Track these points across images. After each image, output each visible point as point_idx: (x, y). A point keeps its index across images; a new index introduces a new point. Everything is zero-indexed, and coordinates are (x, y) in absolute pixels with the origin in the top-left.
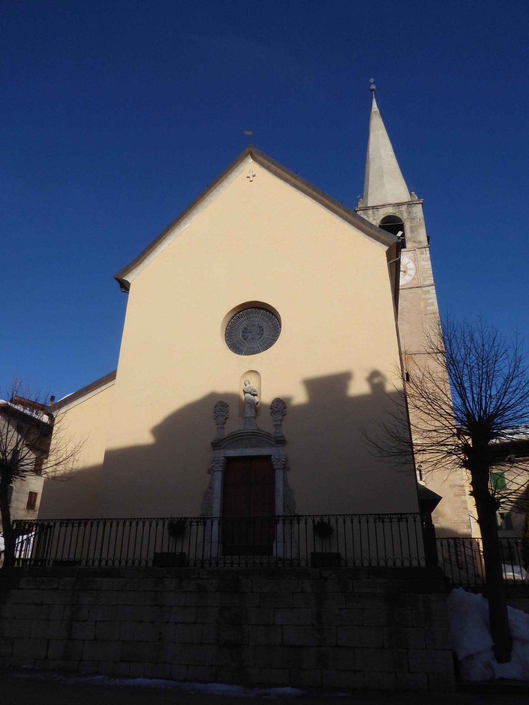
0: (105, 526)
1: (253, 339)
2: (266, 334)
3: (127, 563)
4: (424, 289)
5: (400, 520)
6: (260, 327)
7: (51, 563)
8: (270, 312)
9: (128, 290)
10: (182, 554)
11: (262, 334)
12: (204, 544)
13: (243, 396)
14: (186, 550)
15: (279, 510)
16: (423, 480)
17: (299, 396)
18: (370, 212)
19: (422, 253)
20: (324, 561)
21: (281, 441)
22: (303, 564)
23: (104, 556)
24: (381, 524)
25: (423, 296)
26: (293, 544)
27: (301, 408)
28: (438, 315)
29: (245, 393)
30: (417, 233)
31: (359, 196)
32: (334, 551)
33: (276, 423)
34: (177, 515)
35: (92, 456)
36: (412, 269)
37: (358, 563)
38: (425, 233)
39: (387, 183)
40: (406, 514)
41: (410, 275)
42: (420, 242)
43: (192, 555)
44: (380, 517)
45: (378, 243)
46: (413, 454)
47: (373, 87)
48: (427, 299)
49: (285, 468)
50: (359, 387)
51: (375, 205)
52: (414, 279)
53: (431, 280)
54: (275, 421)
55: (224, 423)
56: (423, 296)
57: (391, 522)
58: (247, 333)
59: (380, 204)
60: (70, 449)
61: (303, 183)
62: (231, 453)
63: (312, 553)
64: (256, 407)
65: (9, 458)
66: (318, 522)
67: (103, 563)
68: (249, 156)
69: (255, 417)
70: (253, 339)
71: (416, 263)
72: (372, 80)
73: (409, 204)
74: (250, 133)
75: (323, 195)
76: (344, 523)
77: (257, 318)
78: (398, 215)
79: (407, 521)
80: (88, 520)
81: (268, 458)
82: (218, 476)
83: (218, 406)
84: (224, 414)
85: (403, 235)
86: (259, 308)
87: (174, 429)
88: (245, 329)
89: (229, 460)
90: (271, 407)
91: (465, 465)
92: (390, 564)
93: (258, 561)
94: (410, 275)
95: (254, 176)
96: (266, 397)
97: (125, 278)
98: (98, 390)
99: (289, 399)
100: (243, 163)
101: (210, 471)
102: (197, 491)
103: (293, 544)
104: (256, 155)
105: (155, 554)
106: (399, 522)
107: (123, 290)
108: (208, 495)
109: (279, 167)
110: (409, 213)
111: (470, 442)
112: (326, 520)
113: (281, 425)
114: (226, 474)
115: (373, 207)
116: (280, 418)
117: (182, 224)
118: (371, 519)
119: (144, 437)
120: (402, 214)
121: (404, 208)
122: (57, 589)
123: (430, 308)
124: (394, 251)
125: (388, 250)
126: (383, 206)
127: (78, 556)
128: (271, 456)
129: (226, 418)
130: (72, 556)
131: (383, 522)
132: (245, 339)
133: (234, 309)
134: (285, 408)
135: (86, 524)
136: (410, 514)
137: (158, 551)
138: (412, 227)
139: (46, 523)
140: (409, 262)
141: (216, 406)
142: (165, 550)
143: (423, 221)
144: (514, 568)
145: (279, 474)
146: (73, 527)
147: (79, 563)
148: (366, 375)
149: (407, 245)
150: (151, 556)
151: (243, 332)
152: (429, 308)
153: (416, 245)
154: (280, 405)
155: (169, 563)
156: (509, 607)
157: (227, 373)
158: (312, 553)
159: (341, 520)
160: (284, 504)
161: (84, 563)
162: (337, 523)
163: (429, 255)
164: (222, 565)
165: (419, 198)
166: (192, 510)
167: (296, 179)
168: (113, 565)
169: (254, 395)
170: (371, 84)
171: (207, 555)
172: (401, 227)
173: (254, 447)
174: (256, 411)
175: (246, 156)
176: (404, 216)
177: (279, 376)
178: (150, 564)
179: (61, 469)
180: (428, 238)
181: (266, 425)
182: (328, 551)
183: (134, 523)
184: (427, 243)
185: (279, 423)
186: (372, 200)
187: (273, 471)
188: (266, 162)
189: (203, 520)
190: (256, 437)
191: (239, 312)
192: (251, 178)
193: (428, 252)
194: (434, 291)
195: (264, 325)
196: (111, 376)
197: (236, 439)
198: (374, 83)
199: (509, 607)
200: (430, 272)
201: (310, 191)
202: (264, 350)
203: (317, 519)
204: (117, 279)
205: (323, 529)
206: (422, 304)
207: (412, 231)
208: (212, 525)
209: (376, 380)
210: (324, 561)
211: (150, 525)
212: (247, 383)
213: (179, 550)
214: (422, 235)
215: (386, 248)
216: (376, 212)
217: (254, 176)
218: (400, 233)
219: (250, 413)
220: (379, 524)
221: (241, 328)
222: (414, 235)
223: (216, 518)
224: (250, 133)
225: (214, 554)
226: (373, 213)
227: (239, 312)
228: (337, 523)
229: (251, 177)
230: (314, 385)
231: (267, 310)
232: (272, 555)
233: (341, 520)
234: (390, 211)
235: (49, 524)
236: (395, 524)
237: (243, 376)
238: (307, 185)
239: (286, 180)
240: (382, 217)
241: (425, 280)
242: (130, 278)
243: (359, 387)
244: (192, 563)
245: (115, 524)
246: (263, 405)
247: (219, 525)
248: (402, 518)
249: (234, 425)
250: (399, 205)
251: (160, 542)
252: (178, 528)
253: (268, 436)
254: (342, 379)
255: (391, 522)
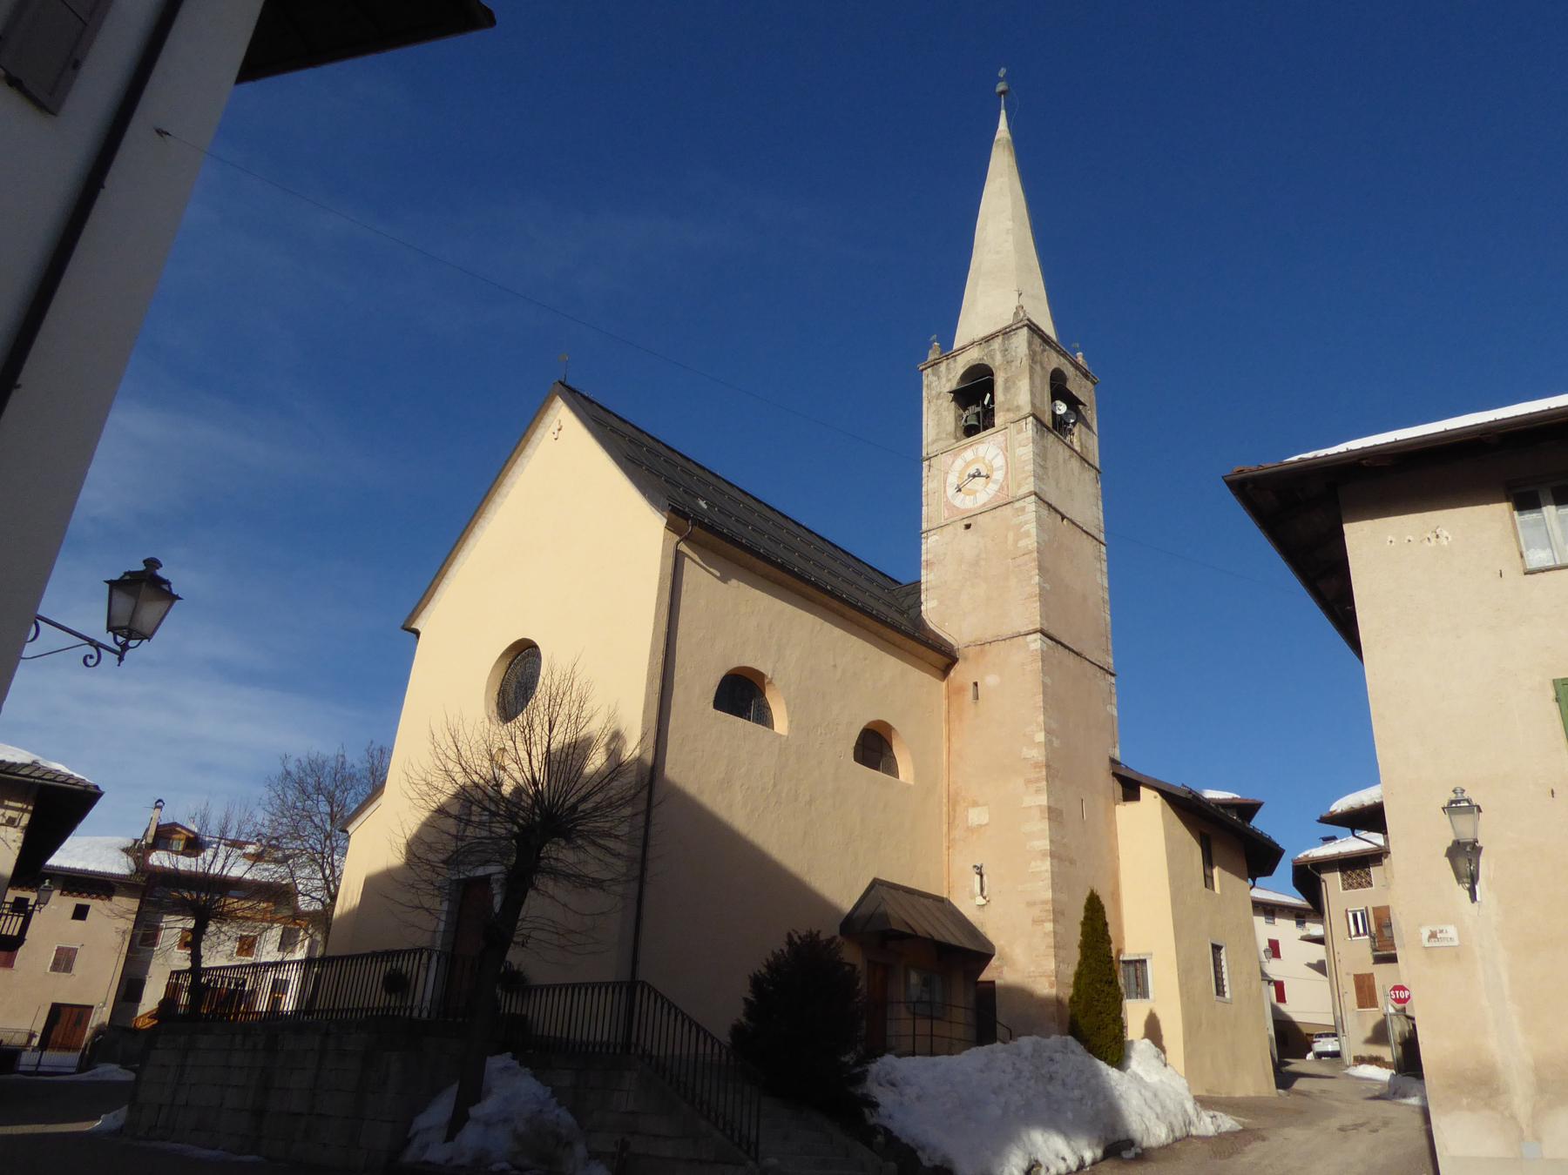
0: (430, 958)
4: (1017, 505)
19: (1020, 431)
25: (1016, 521)
41: (996, 482)
42: (1018, 408)
46: (1053, 900)
48: (1020, 526)
52: (1001, 488)
78: (987, 361)
94: (996, 482)
120: (993, 358)
121: (997, 344)
138: (1006, 380)
144: (115, 597)
153: (1011, 416)
156: (126, 1107)
199: (126, 1107)
206: (1011, 536)
207: (1007, 389)
240: (961, 371)
241: (1019, 487)
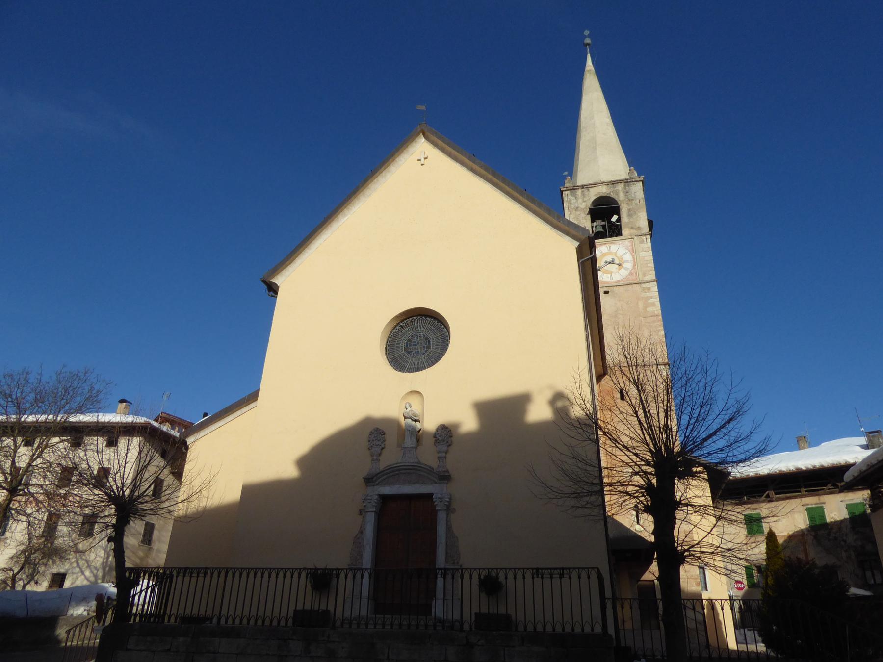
1: (418, 353)
2: (433, 347)
3: (264, 621)
4: (644, 286)
5: (561, 576)
6: (427, 339)
7: (172, 620)
8: (439, 321)
9: (276, 293)
10: (327, 611)
11: (428, 347)
12: (353, 600)
13: (403, 422)
14: (331, 608)
15: (441, 561)
16: (641, 522)
17: (469, 423)
18: (579, 192)
19: (642, 242)
20: (494, 625)
21: (445, 477)
22: (466, 627)
23: (224, 612)
24: (540, 579)
25: (643, 295)
26: (455, 602)
27: (470, 436)
28: (661, 317)
29: (405, 418)
30: (635, 215)
31: (566, 173)
32: (502, 611)
33: (440, 455)
34: (321, 565)
35: (226, 491)
36: (629, 261)
37: (540, 628)
38: (646, 217)
39: (601, 156)
40: (569, 569)
41: (626, 269)
42: (639, 228)
43: (339, 614)
44: (537, 572)
45: (567, 238)
47: (588, 41)
48: (648, 298)
49: (449, 509)
50: (539, 412)
51: (585, 183)
52: (631, 274)
53: (652, 275)
54: (438, 452)
55: (380, 454)
56: (643, 295)
57: (551, 578)
58: (411, 345)
59: (591, 182)
60: (197, 483)
61: (481, 167)
62: (387, 490)
63: (476, 614)
64: (417, 436)
65: (127, 493)
66: (485, 576)
67: (223, 621)
68: (421, 135)
69: (416, 448)
70: (418, 353)
71: (626, 259)
72: (587, 33)
73: (627, 182)
74: (423, 108)
75: (504, 181)
76: (515, 578)
77: (424, 328)
78: (613, 195)
79: (570, 578)
80: (209, 569)
81: (429, 497)
82: (371, 518)
83: (374, 433)
84: (379, 443)
85: (619, 220)
86: (426, 316)
87: (320, 460)
88: (409, 340)
89: (385, 499)
90: (435, 435)
91: (648, 510)
92: (549, 628)
93: (405, 623)
94: (626, 269)
95: (426, 158)
96: (430, 424)
97: (273, 280)
98: (239, 413)
99: (456, 426)
100: (414, 144)
101: (362, 512)
102: (344, 538)
103: (455, 602)
104: (427, 134)
105: (295, 611)
106: (561, 578)
107: (272, 293)
108: (358, 541)
109: (454, 148)
110: (626, 193)
111: (654, 481)
112: (494, 574)
113: (445, 457)
114: (381, 515)
115: (583, 187)
116: (445, 448)
117: (340, 216)
118: (528, 575)
119: (289, 471)
120: (617, 194)
121: (620, 187)
122: (169, 650)
123: (649, 309)
124: (587, 247)
125: (579, 246)
126: (595, 185)
127: (209, 612)
128: (432, 494)
129: (383, 448)
130: (202, 612)
131: (542, 578)
132: (409, 353)
133: (397, 317)
134: (451, 437)
135: (205, 574)
136: (574, 568)
137: (300, 607)
138: (629, 210)
139: (168, 572)
140: (626, 253)
141: (371, 433)
142: (308, 606)
143: (643, 202)
145: (442, 517)
146: (191, 577)
147: (206, 619)
148: (549, 395)
149: (623, 232)
150: (291, 614)
151: (407, 344)
152: (649, 309)
153: (634, 232)
154: (446, 433)
155: (310, 622)
157: (386, 394)
158: (476, 614)
159: (511, 575)
160: (447, 553)
161: (215, 620)
162: (506, 578)
163: (650, 245)
164: (389, 627)
165: (639, 174)
166: (336, 558)
167: (474, 162)
168: (234, 623)
169: (415, 421)
170: (586, 37)
171: (356, 613)
172: (617, 211)
173: (414, 483)
174: (418, 441)
175: (418, 135)
176: (621, 197)
177: (444, 397)
178: (290, 623)
179: (195, 506)
180: (651, 224)
181: (428, 457)
182: (496, 612)
183: (259, 574)
184: (648, 230)
185: (444, 454)
186: (582, 178)
187: (434, 513)
188: (440, 142)
189: (355, 570)
190: (415, 471)
191: (403, 321)
192: (422, 161)
193: (649, 240)
194: (656, 289)
195: (431, 336)
196: (253, 397)
197: (393, 473)
198: (589, 36)
200: (652, 265)
201: (490, 176)
202: (430, 366)
203: (484, 573)
204: (264, 282)
205: (491, 585)
206: (641, 304)
207: (630, 215)
208: (362, 578)
209: (560, 404)
210: (494, 625)
211: (292, 577)
212: (408, 406)
213: (323, 607)
214: (642, 220)
215: (577, 244)
216: (586, 192)
217: (426, 158)
218: (614, 218)
219: (409, 442)
220: (538, 581)
221: (404, 340)
222: (632, 220)
223: (366, 569)
224: (423, 108)
225: (364, 613)
226: (583, 194)
227: (403, 321)
228: (506, 578)
229: (423, 159)
230: (485, 409)
231: (435, 319)
232: (431, 615)
233: (511, 575)
234: (603, 190)
235: (171, 573)
236: (556, 581)
237: (404, 398)
238: (486, 170)
239: (463, 164)
240: (594, 198)
241: (644, 275)
242: (278, 280)
243: (539, 412)
244: (338, 623)
245: (289, 575)
246: (426, 433)
247: (370, 578)
248: (563, 574)
249: (390, 457)
250: (614, 183)
251: (302, 597)
252: (322, 580)
253: (431, 470)
254: (521, 401)
255: (551, 578)
